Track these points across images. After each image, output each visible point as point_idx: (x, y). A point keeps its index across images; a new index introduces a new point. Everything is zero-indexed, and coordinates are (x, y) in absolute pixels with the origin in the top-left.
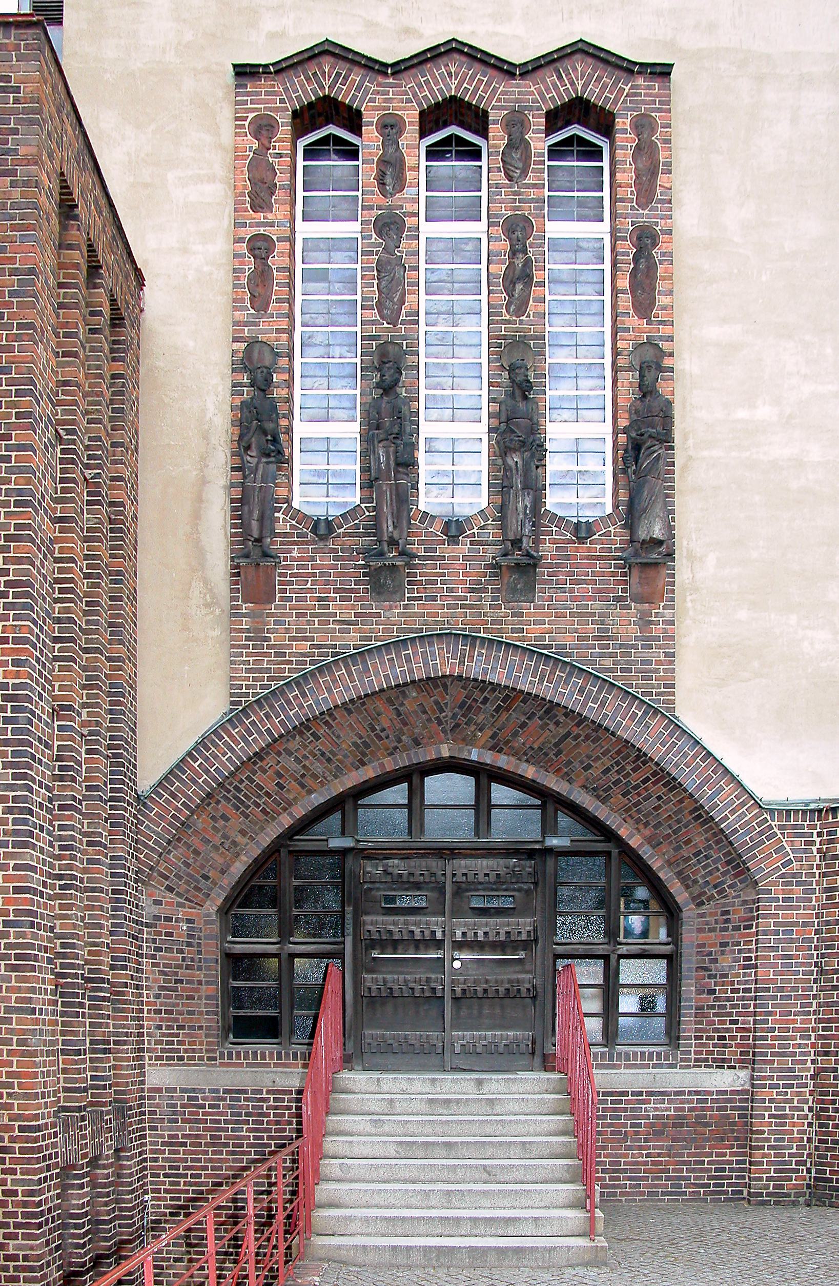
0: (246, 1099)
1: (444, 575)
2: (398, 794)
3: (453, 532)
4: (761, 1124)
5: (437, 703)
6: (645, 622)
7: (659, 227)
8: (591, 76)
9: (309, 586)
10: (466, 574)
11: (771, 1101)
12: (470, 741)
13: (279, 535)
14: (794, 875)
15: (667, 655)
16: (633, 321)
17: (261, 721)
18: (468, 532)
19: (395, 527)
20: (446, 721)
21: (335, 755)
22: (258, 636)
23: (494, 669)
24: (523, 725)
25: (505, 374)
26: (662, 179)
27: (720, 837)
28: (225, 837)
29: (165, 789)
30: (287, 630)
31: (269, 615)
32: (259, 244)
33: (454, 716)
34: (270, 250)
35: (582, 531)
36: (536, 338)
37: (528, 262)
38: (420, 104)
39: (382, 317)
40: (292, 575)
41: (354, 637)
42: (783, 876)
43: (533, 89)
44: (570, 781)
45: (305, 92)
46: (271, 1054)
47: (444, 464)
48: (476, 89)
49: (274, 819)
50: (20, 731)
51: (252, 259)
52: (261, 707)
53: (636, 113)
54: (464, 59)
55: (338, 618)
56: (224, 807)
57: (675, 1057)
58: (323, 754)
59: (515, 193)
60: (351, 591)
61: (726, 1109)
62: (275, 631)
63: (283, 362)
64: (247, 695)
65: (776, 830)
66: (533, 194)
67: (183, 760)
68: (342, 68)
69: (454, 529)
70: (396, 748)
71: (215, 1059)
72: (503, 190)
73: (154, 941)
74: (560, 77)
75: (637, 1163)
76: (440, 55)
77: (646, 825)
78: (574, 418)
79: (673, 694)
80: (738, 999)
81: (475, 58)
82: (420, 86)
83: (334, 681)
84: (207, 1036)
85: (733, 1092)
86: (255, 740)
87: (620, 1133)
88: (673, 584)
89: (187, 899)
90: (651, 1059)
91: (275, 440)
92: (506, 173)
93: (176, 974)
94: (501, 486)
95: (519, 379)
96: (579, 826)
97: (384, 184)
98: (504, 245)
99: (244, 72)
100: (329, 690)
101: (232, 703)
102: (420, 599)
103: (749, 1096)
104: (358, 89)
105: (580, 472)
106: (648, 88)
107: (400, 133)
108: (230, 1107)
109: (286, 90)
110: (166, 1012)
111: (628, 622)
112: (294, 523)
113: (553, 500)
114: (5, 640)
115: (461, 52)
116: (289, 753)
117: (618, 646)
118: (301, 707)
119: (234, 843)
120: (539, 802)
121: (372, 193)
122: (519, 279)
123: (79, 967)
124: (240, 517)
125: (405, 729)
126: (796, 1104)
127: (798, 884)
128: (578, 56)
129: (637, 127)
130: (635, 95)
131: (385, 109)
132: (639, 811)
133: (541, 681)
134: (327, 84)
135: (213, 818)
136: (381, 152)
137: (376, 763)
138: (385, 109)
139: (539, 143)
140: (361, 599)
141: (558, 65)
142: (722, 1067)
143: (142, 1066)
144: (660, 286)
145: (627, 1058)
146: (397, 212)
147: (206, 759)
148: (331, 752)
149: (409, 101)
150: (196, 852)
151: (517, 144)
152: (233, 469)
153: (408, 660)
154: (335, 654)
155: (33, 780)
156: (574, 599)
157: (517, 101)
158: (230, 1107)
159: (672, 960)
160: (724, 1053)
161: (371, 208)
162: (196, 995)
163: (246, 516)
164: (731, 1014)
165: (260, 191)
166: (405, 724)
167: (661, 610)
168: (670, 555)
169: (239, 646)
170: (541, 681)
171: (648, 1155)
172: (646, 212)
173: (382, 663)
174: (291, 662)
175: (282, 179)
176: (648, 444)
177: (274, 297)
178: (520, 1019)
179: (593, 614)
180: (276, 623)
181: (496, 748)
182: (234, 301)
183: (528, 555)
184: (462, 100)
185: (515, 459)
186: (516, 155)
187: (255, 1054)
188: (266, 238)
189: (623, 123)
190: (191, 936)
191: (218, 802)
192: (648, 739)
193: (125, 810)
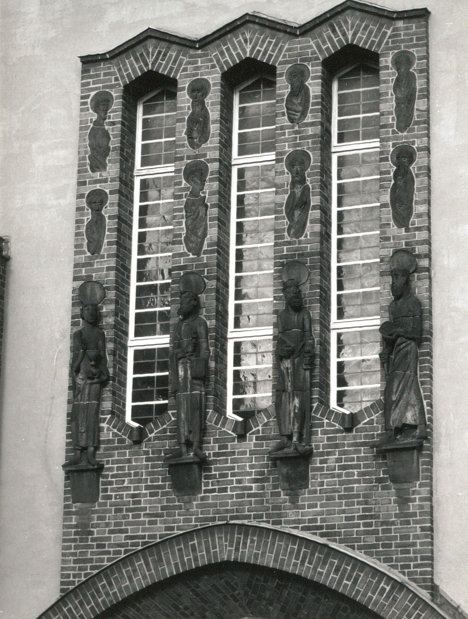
1: (233, 468)
5: (227, 583)
6: (403, 500)
7: (416, 145)
8: (359, 26)
9: (125, 484)
10: (251, 467)
13: (104, 442)
16: (394, 230)
17: (76, 608)
18: (254, 430)
19: (190, 432)
20: (241, 598)
22: (83, 530)
23: (264, 553)
24: (302, 600)
26: (419, 104)
33: (246, 593)
38: (221, 68)
39: (189, 250)
40: (113, 476)
41: (160, 528)
43: (312, 43)
45: (134, 70)
51: (90, 211)
52: (76, 597)
53: (396, 51)
54: (257, 27)
55: (148, 512)
59: (296, 132)
60: (159, 487)
62: (97, 526)
72: (287, 131)
74: (334, 31)
82: (222, 53)
83: (135, 571)
92: (289, 117)
97: (192, 138)
99: (89, 62)
100: (130, 579)
102: (213, 491)
105: (354, 332)
106: (407, 28)
107: (205, 94)
109: (120, 70)
111: (388, 501)
112: (115, 431)
115: (254, 23)
117: (379, 524)
118: (107, 594)
121: (183, 146)
125: (206, 606)
128: (348, 12)
129: (396, 64)
133: (303, 562)
134: (150, 61)
136: (190, 112)
140: (167, 494)
141: (332, 21)
146: (202, 160)
149: (213, 66)
151: (299, 91)
156: (341, 483)
157: (299, 55)
161: (182, 159)
167: (417, 488)
170: (303, 562)
172: (405, 133)
173: (173, 553)
176: (399, 341)
177: (106, 241)
179: (358, 496)
180: (99, 518)
182: (76, 246)
185: (287, 364)
186: (297, 101)
189: (387, 60)
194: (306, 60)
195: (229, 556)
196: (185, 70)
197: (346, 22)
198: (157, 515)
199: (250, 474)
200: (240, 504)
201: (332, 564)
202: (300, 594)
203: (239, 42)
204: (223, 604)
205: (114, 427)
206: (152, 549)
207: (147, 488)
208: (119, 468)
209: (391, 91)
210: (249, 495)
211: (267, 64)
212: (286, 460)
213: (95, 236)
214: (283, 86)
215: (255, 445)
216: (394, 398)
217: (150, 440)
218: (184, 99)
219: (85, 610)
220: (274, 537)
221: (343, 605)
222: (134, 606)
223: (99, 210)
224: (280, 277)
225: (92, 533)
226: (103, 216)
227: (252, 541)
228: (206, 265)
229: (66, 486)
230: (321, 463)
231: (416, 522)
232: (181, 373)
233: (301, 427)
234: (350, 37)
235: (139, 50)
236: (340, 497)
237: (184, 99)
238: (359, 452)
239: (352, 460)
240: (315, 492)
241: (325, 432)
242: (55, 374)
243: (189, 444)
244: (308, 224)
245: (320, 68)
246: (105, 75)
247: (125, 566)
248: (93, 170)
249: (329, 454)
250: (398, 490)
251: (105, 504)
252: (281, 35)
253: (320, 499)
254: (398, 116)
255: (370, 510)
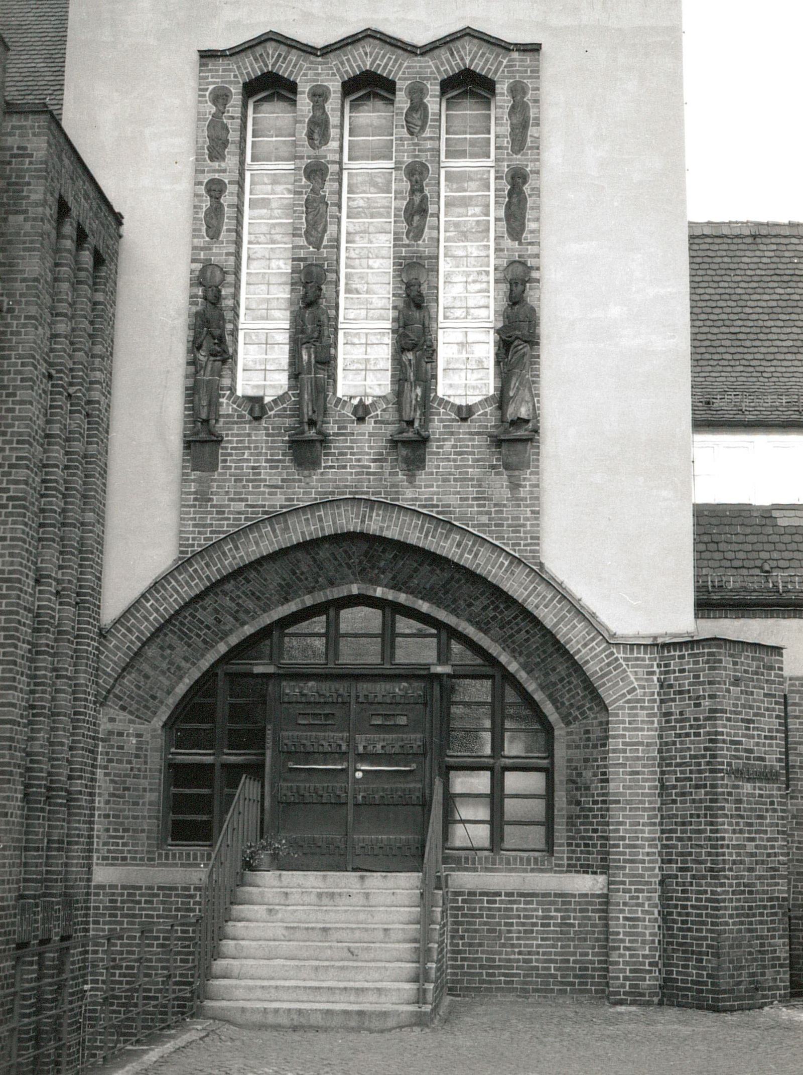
0: (177, 896)
1: (352, 448)
2: (319, 624)
3: (360, 413)
4: (617, 926)
6: (515, 486)
8: (476, 53)
10: (370, 448)
11: (625, 904)
12: (375, 582)
14: (638, 701)
15: (533, 512)
16: (508, 243)
17: (202, 569)
19: (314, 412)
21: (263, 594)
22: (203, 497)
25: (404, 287)
26: (532, 131)
27: (577, 668)
28: (171, 663)
29: (123, 625)
30: (227, 493)
31: (212, 480)
32: (214, 187)
33: (360, 562)
34: (221, 191)
35: (464, 414)
36: (430, 258)
37: (424, 199)
39: (310, 243)
40: (232, 448)
42: (628, 702)
44: (458, 616)
45: (253, 69)
46: (202, 855)
47: (357, 353)
48: (386, 65)
49: (212, 647)
50: (12, 604)
52: (203, 558)
54: (377, 42)
56: (172, 639)
57: (550, 862)
58: (253, 594)
60: (279, 461)
61: (587, 911)
62: (217, 493)
63: (230, 278)
64: (193, 546)
65: (621, 661)
66: (429, 144)
67: (138, 601)
68: (283, 49)
69: (362, 413)
70: (314, 588)
71: (153, 859)
73: (107, 753)
74: (452, 54)
75: (509, 960)
76: (359, 40)
77: (521, 654)
78: (464, 314)
79: (538, 544)
80: (598, 809)
81: (385, 42)
82: (342, 63)
83: (261, 536)
84: (148, 838)
85: (593, 895)
86: (196, 585)
87: (494, 931)
88: (538, 454)
89: (137, 717)
90: (529, 863)
91: (221, 340)
93: (125, 782)
94: (400, 380)
95: (413, 294)
96: (469, 653)
98: (406, 185)
99: (207, 55)
100: (257, 544)
101: (181, 552)
103: (606, 899)
104: (295, 66)
106: (522, 60)
107: (326, 99)
108: (163, 902)
109: (239, 68)
110: (114, 816)
113: (442, 389)
114: (3, 539)
116: (225, 594)
118: (234, 558)
119: (179, 668)
120: (434, 631)
121: (303, 146)
122: (417, 212)
123: (42, 778)
124: (192, 402)
125: (321, 573)
126: (646, 908)
127: (642, 708)
128: (466, 38)
130: (511, 66)
131: (314, 81)
132: (513, 642)
133: (426, 536)
134: (270, 62)
135: (162, 648)
137: (298, 600)
138: (314, 81)
139: (433, 103)
141: (451, 45)
142: (587, 873)
143: (90, 866)
144: (530, 214)
145: (508, 863)
147: (157, 600)
148: (260, 591)
149: (334, 75)
150: (147, 677)
151: (418, 107)
152: (188, 364)
153: (321, 520)
154: (265, 513)
155: (18, 639)
156: (457, 467)
157: (417, 73)
158: (163, 902)
159: (549, 772)
160: (588, 859)
161: (302, 158)
162: (141, 801)
163: (197, 402)
164: (592, 824)
165: (216, 144)
166: (321, 569)
168: (536, 431)
169: (188, 506)
170: (426, 536)
171: (520, 953)
172: (519, 156)
174: (228, 519)
175: (233, 136)
176: (516, 343)
177: (225, 228)
178: (396, 827)
179: (472, 480)
180: (218, 487)
181: (395, 587)
182: (194, 230)
183: (418, 433)
184: (375, 74)
186: (417, 116)
187: (188, 855)
188: (220, 182)
189: (502, 88)
190: (138, 749)
191: (166, 635)
192: (516, 585)
193: (89, 645)
194: (425, 79)
195: (355, 527)
196: (305, 75)
197: (464, 48)
198: (276, 487)
199: (369, 454)
200: (359, 481)
201: (454, 539)
202: (415, 565)
203: (359, 54)
204: (337, 571)
205: (234, 403)
206: (275, 517)
207: (267, 461)
208: (238, 442)
209: (506, 116)
210: (368, 474)
211: (386, 79)
212: (406, 443)
213: (214, 222)
214: (402, 100)
215: (374, 428)
216: (511, 394)
217: (269, 417)
218: (304, 103)
219: (211, 571)
220: (399, 513)
221: (457, 576)
222: (255, 569)
223: (218, 198)
224: (400, 276)
225: (211, 500)
226: (222, 205)
227: (378, 515)
228: (325, 259)
229: (184, 454)
230: (438, 447)
231: (527, 506)
232: (305, 357)
233: (423, 414)
234: (467, 62)
235: (259, 50)
236: (455, 480)
237: (304, 103)
238: (474, 440)
239: (468, 447)
240: (432, 474)
241: (441, 421)
242: (171, 350)
243: (312, 423)
244: (426, 230)
245: (438, 88)
246: (224, 71)
247: (252, 532)
248: (212, 159)
249: (444, 440)
250: (509, 476)
251: (225, 474)
252: (400, 52)
253: (437, 480)
254: (513, 140)
255: (484, 492)
